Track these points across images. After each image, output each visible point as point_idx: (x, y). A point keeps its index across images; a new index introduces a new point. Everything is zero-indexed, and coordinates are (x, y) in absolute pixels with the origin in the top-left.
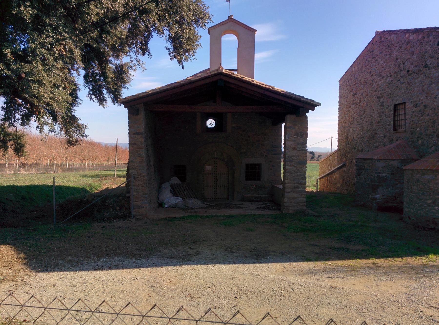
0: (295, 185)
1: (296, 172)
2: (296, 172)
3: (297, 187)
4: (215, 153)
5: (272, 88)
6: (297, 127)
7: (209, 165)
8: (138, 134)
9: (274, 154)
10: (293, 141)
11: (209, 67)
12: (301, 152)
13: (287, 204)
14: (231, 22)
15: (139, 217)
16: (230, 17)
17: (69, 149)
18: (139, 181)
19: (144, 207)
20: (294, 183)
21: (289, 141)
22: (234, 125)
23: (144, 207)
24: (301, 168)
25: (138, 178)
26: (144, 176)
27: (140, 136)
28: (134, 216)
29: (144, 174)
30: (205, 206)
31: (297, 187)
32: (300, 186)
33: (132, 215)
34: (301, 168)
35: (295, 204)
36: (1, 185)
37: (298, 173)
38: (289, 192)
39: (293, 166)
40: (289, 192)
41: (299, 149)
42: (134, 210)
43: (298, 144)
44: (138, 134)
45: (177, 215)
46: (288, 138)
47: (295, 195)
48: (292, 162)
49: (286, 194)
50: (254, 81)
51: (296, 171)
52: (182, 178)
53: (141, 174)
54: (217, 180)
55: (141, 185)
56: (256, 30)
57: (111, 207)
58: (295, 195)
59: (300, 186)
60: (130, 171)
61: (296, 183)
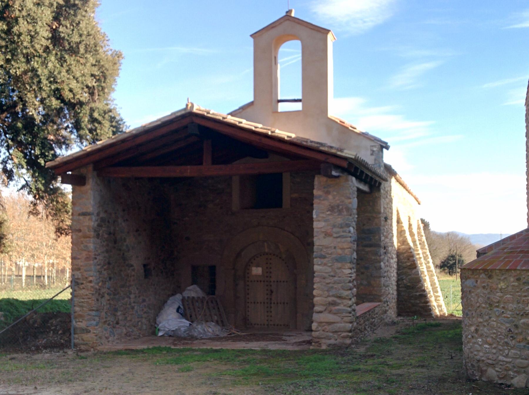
0: (330, 299)
1: (332, 276)
2: (332, 276)
3: (334, 304)
4: (266, 244)
5: (272, 132)
6: (330, 197)
7: (258, 266)
8: (84, 214)
9: (366, 246)
10: (325, 221)
11: (251, 99)
12: (339, 240)
13: (317, 333)
14: (288, 22)
15: (83, 347)
16: (288, 14)
17: (59, 240)
18: (84, 288)
19: (90, 332)
20: (329, 296)
21: (319, 221)
22: (295, 195)
23: (90, 332)
24: (340, 268)
25: (82, 284)
26: (91, 282)
27: (88, 217)
28: (76, 345)
29: (91, 279)
30: (225, 335)
31: (334, 304)
32: (338, 301)
33: (72, 344)
34: (340, 268)
35: (331, 334)
36: (3, 300)
37: (336, 278)
38: (321, 312)
39: (325, 264)
40: (321, 312)
41: (335, 235)
42: (76, 336)
43: (334, 226)
44: (84, 214)
45: (140, 347)
46: (317, 215)
47: (330, 317)
48: (324, 257)
49: (315, 316)
50: (241, 123)
51: (332, 274)
52: (211, 290)
53: (86, 278)
54: (272, 292)
55: (87, 295)
56: (329, 31)
57: (52, 330)
58: (330, 317)
59: (338, 301)
60: (465, 290)
61: (333, 296)
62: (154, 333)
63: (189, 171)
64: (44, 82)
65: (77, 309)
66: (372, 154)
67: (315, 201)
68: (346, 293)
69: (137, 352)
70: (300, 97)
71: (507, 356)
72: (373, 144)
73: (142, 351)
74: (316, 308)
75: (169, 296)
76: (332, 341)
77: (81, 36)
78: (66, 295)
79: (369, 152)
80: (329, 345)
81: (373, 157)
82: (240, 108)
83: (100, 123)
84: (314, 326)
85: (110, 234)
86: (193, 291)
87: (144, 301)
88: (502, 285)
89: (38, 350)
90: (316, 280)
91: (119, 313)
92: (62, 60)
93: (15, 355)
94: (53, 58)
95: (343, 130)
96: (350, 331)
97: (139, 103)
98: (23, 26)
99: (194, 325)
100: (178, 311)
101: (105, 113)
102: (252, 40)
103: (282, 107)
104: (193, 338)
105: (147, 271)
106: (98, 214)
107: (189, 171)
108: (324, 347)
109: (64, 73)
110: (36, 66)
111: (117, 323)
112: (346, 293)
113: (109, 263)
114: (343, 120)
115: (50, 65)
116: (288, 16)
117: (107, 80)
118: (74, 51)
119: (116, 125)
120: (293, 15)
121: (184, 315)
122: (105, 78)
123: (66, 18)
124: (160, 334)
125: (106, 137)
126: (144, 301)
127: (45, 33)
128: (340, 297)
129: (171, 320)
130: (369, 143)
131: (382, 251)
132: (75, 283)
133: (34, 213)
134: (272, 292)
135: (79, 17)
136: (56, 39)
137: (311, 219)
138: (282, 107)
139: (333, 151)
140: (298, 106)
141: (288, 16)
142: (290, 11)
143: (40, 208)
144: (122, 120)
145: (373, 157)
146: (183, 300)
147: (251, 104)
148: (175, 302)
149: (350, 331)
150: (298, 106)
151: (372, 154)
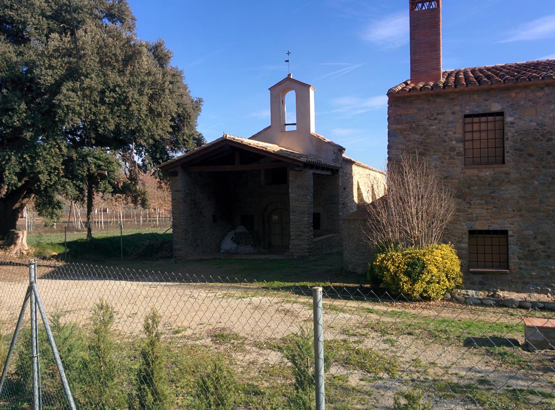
0: (298, 233)
3: (300, 235)
8: (177, 191)
28: (175, 257)
31: (300, 235)
44: (177, 191)
45: (206, 258)
49: (291, 242)
59: (302, 234)
62: (219, 251)
63: (228, 168)
64: (145, 132)
65: (176, 239)
66: (334, 154)
67: (290, 183)
68: (305, 230)
69: (204, 260)
70: (295, 122)
71: (355, 259)
72: (334, 148)
73: (207, 260)
74: (292, 238)
75: (229, 231)
76: (299, 254)
77: (162, 108)
78: (171, 231)
79: (333, 153)
80: (298, 256)
81: (335, 155)
82: (264, 130)
83: (187, 141)
84: (291, 246)
85: (192, 200)
86: (241, 229)
87: (213, 234)
88: (353, 226)
89: (157, 259)
90: (291, 223)
91: (198, 241)
92: (153, 120)
93: (145, 262)
94: (149, 120)
95: (319, 142)
96: (308, 249)
97: (210, 128)
98: (134, 107)
99: (239, 246)
100: (232, 239)
101: (190, 136)
102: (269, 91)
103: (288, 128)
104: (237, 253)
105: (215, 219)
106: (185, 191)
107: (228, 168)
108: (295, 257)
109: (154, 127)
110: (141, 124)
111: (197, 246)
112: (305, 230)
113: (192, 216)
114: (318, 135)
115: (148, 123)
116: (288, 78)
117: (192, 118)
118: (159, 115)
119: (199, 140)
120: (291, 77)
121: (235, 242)
122: (190, 117)
123: (155, 99)
124: (222, 251)
125: (193, 147)
126: (213, 234)
127: (144, 108)
128: (303, 232)
129: (228, 244)
130: (332, 148)
131: (340, 206)
132: (174, 226)
133: (160, 187)
134: (283, 229)
135: (162, 98)
136: (151, 110)
137: (289, 193)
138: (288, 128)
139: (295, 158)
140: (294, 128)
141: (288, 78)
142: (289, 75)
143: (163, 184)
144: (203, 137)
145: (335, 155)
146: (235, 234)
147: (270, 127)
148: (232, 234)
149: (308, 249)
150: (294, 128)
151: (334, 154)
